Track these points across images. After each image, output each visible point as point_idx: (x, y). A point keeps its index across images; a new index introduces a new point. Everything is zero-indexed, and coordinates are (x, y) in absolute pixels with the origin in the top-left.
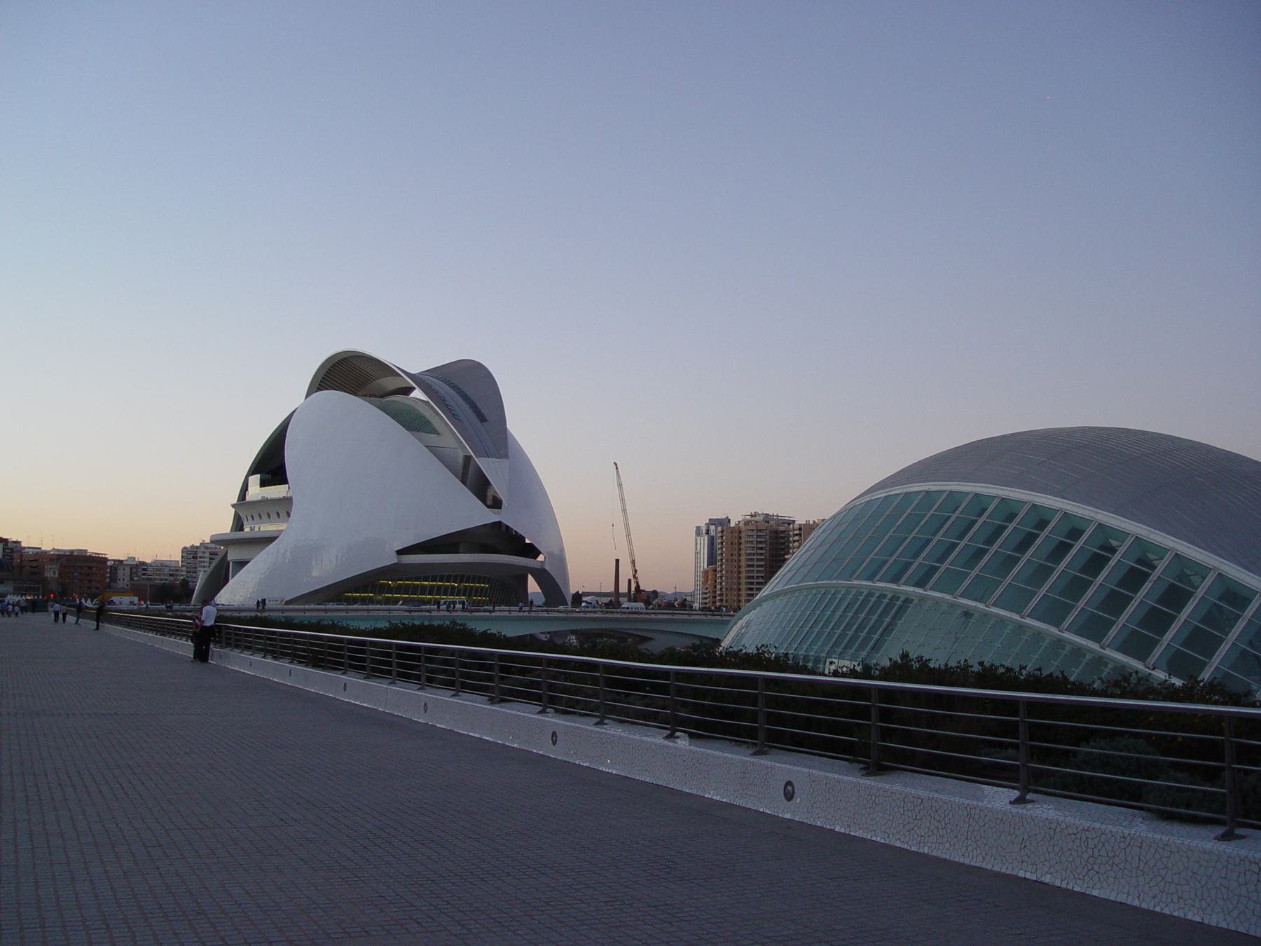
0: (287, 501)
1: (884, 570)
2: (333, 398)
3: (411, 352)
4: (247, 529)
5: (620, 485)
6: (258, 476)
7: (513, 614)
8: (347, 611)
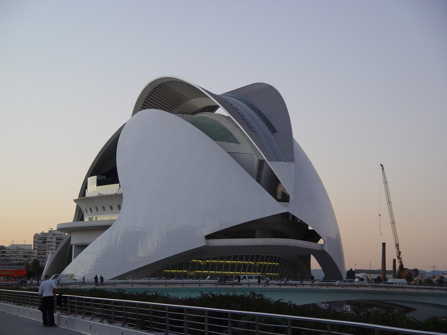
0: (118, 197)
3: (216, 78)
4: (86, 219)
6: (95, 178)
8: (166, 284)
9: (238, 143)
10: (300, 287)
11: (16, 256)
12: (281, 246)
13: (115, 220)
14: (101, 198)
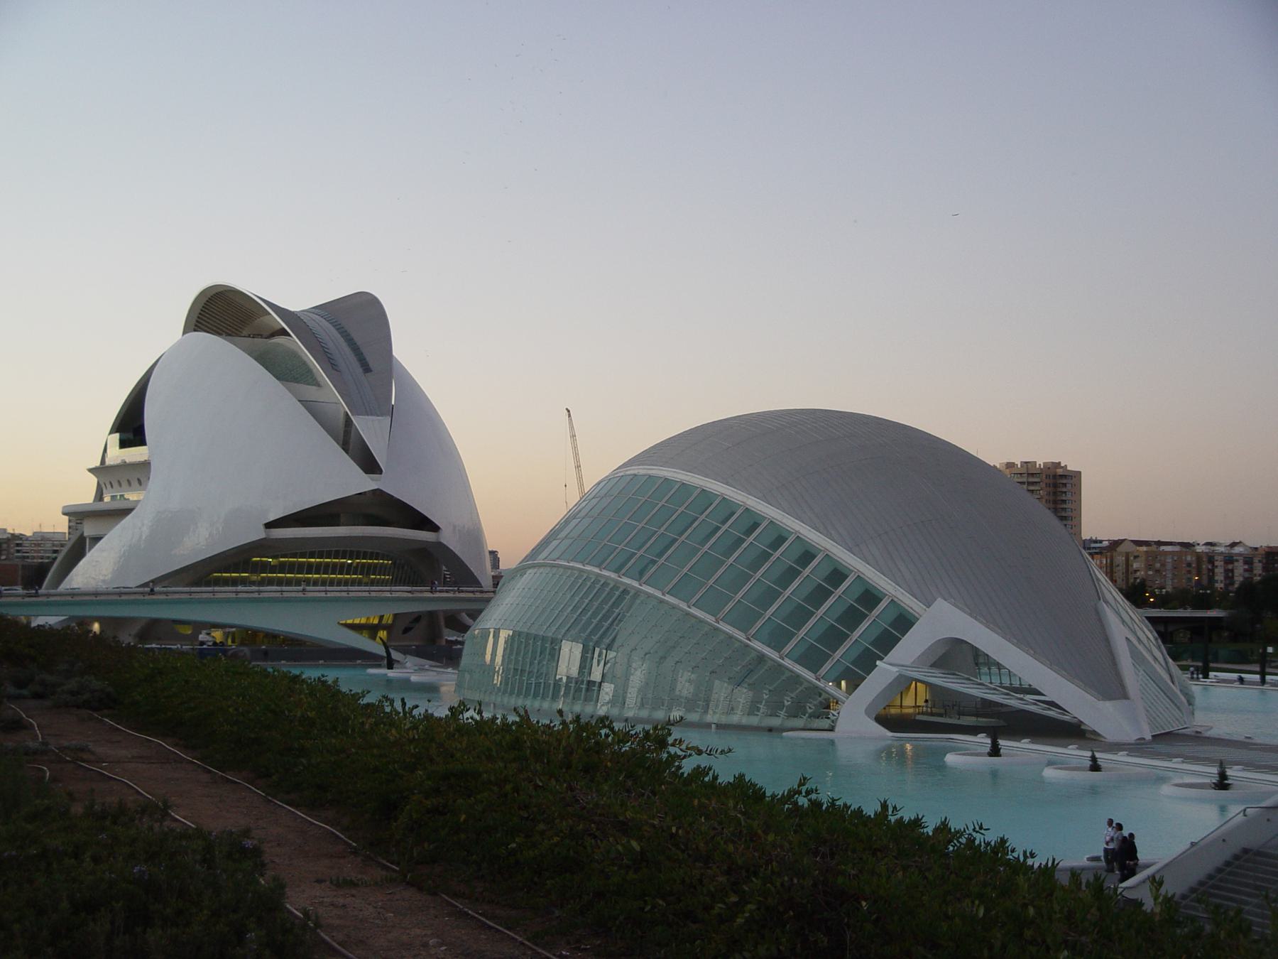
0: (145, 465)
2: (204, 338)
3: (292, 284)
4: (107, 499)
5: (573, 436)
6: (117, 435)
8: (166, 593)
9: (319, 385)
10: (458, 595)
11: (38, 551)
13: (138, 501)
14: (124, 466)
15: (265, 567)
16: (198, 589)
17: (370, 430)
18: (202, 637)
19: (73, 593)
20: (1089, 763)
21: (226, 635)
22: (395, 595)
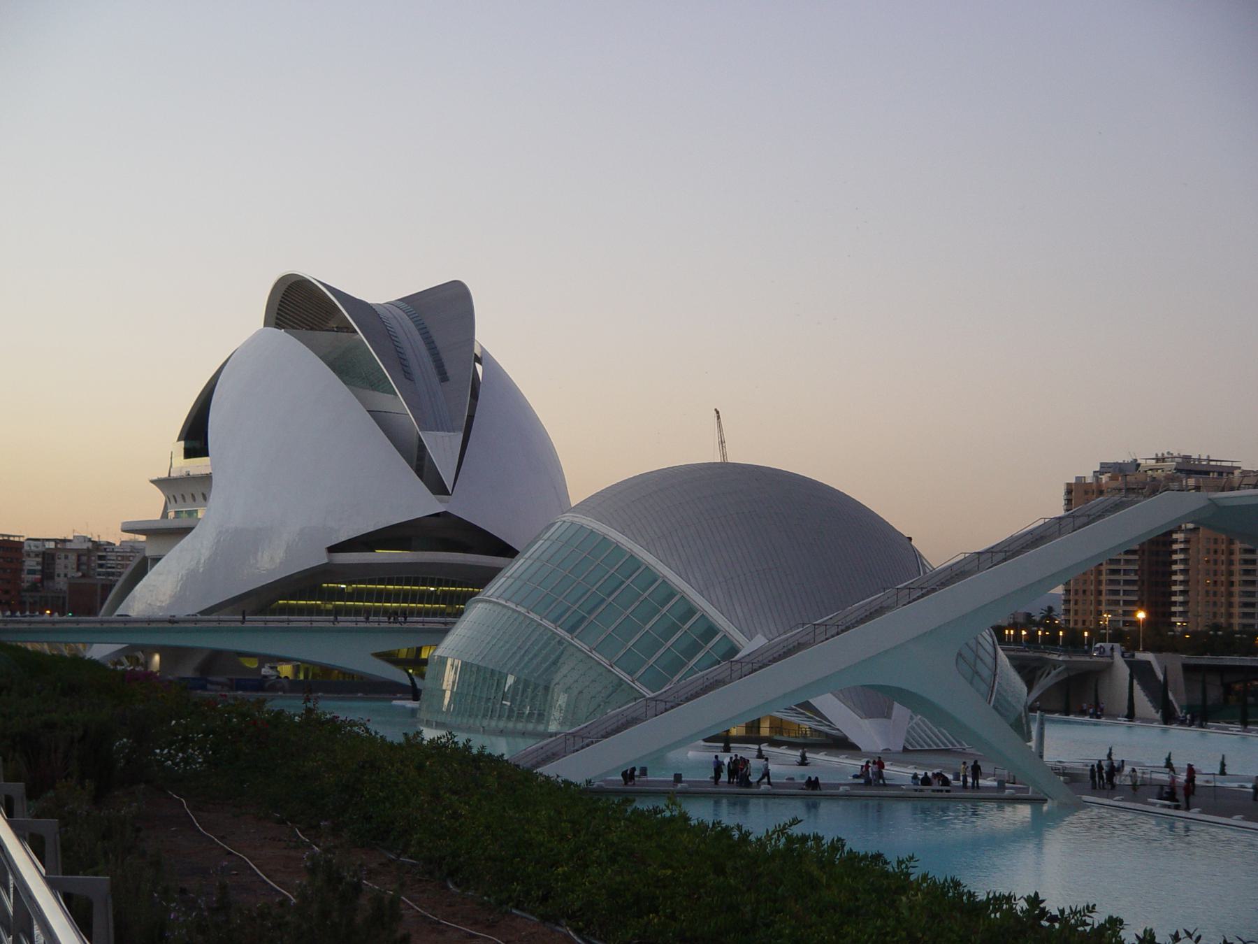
0: (207, 479)
1: (651, 589)
2: (281, 336)
3: (377, 277)
4: (171, 514)
5: (722, 442)
7: (383, 625)
12: (1249, 506)
14: (188, 479)
15: (341, 595)
16: (272, 618)
17: (442, 449)
18: (265, 671)
19: (126, 620)
20: (799, 759)
21: (296, 670)
22: (427, 626)
